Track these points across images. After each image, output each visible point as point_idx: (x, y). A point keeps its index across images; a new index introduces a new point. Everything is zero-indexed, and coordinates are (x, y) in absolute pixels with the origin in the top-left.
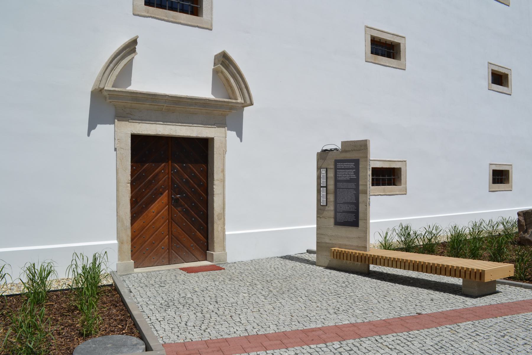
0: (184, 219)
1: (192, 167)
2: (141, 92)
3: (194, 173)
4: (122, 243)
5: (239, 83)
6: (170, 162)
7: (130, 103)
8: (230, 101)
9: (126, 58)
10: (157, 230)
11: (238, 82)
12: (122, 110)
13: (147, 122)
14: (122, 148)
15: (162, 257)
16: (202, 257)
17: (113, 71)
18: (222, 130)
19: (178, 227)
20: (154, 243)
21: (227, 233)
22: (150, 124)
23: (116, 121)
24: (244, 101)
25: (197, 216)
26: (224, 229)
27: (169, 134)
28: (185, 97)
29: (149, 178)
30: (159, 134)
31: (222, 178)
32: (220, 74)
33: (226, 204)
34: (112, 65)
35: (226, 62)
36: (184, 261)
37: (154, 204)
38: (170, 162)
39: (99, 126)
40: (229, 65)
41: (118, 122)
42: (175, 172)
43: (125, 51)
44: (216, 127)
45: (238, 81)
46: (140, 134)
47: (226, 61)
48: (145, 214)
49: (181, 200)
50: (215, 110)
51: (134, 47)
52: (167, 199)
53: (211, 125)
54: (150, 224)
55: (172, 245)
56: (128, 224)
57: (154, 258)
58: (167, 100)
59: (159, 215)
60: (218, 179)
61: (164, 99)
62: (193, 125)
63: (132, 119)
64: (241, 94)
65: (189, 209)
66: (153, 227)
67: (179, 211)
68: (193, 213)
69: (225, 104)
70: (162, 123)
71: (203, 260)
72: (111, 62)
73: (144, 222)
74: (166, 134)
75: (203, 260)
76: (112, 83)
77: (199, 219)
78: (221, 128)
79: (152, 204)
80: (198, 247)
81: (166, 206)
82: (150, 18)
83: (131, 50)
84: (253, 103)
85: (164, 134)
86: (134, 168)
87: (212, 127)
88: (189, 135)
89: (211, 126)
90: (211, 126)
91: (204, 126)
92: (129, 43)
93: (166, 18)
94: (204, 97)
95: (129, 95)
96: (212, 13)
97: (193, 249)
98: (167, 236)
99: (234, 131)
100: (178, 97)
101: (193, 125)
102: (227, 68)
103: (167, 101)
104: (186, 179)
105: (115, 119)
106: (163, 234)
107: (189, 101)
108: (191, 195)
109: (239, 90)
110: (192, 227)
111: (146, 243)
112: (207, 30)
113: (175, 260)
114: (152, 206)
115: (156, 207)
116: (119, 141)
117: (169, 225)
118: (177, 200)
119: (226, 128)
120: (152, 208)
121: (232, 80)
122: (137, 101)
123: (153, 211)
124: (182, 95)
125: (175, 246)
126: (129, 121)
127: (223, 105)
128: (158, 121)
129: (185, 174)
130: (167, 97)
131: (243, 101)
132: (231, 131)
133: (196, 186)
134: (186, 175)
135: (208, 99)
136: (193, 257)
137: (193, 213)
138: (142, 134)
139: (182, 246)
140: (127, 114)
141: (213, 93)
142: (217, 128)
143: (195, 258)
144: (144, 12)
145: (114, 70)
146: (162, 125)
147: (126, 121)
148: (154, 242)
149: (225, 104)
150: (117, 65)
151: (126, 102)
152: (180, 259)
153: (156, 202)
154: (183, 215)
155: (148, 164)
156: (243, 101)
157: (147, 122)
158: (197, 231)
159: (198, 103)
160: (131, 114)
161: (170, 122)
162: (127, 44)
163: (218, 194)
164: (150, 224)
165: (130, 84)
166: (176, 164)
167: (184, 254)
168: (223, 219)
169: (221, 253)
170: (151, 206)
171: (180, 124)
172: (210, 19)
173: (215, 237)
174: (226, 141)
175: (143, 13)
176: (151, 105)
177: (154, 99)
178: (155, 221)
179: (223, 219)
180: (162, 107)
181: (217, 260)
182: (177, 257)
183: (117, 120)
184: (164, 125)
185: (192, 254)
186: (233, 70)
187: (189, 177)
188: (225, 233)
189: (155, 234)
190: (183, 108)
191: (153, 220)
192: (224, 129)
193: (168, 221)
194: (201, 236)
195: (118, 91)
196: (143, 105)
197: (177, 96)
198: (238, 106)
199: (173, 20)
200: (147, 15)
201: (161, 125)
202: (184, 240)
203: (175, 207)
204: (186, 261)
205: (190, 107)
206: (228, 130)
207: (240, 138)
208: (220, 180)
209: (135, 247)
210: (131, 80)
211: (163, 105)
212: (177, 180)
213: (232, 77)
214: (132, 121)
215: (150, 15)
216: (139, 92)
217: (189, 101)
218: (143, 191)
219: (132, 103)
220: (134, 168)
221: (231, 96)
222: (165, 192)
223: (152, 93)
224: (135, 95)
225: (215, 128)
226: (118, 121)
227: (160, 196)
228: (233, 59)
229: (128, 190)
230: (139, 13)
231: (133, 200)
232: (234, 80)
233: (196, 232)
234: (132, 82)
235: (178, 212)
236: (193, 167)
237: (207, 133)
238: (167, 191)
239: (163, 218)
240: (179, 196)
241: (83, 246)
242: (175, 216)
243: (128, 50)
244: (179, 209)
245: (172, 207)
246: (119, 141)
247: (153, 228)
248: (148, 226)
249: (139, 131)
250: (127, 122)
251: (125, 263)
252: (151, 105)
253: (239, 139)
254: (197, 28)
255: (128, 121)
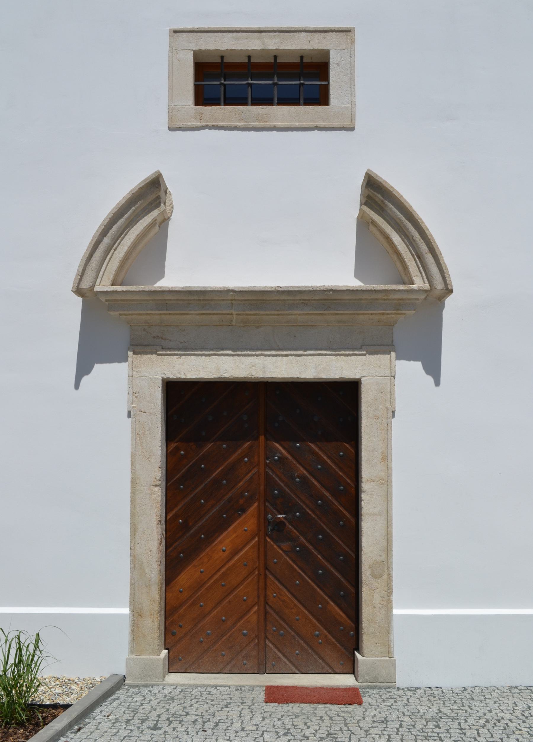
0: (296, 570)
1: (317, 450)
2: (171, 290)
3: (323, 463)
4: (140, 616)
5: (413, 242)
6: (262, 438)
7: (157, 314)
8: (389, 288)
9: (141, 221)
10: (232, 592)
11: (412, 241)
12: (144, 330)
13: (196, 353)
14: (143, 410)
15: (244, 653)
16: (342, 665)
17: (112, 251)
18: (384, 359)
19: (281, 587)
20: (223, 621)
21: (396, 612)
22: (204, 357)
23: (130, 353)
24: (430, 286)
25: (329, 566)
26: (390, 601)
27: (249, 376)
28: (274, 289)
29: (214, 475)
30: (225, 378)
31: (383, 474)
32: (372, 227)
33: (394, 539)
34: (106, 240)
35: (376, 196)
36: (296, 668)
37: (226, 533)
38: (262, 438)
39: (98, 368)
40: (384, 203)
41: (135, 356)
42: (275, 461)
43: (133, 208)
44: (365, 352)
45: (411, 237)
46: (183, 378)
47: (375, 193)
48: (204, 554)
49: (290, 527)
50: (358, 314)
51: (154, 196)
52: (256, 522)
53: (353, 349)
54: (215, 577)
55: (267, 628)
56: (153, 575)
57: (223, 656)
58: (236, 300)
59: (236, 558)
60: (373, 478)
61: (228, 300)
62: (305, 353)
63: (163, 349)
64: (421, 269)
65: (310, 547)
66: (223, 583)
67: (284, 551)
68: (319, 556)
69: (379, 296)
70: (230, 352)
71: (345, 671)
72: (104, 233)
73: (201, 572)
74: (242, 376)
75: (345, 671)
76: (111, 277)
77: (336, 574)
78: (380, 356)
79: (221, 533)
80: (333, 640)
81: (253, 538)
82: (207, 131)
83: (150, 204)
84: (451, 285)
85: (236, 376)
86: (182, 452)
87: (356, 355)
88: (296, 376)
89: (351, 353)
90: (351, 353)
91: (333, 353)
92: (142, 188)
93: (241, 124)
94: (322, 284)
95: (148, 298)
96: (353, 90)
97: (320, 644)
98: (256, 608)
99: (415, 360)
100: (255, 291)
101: (305, 353)
102: (380, 210)
103: (234, 302)
104: (303, 478)
105: (129, 349)
106: (245, 601)
107: (284, 297)
108: (315, 514)
109: (415, 260)
110: (318, 590)
111: (207, 619)
112: (343, 132)
113: (273, 666)
114: (221, 537)
115: (230, 540)
116: (136, 397)
117: (258, 582)
118: (279, 525)
119: (393, 354)
120: (220, 542)
121: (396, 238)
122: (167, 310)
123: (224, 548)
124: (265, 287)
125: (274, 630)
126: (158, 353)
127: (377, 299)
128: (223, 349)
129: (298, 466)
130: (231, 293)
131: (427, 286)
132: (409, 359)
133: (327, 494)
134: (302, 469)
135: (332, 290)
136: (321, 661)
137: (319, 556)
138: (186, 378)
139: (293, 633)
140: (154, 337)
141: (358, 275)
142: (367, 356)
143: (323, 664)
144: (193, 119)
145: (115, 250)
146: (232, 358)
147: (152, 354)
148: (224, 618)
149: (379, 296)
150: (120, 239)
151: (147, 314)
152: (286, 663)
153: (230, 529)
154: (294, 562)
155: (212, 444)
156: (427, 286)
157: (196, 353)
158: (329, 600)
159: (309, 300)
160: (163, 339)
161: (250, 349)
162: (135, 191)
163: (373, 514)
164: (215, 577)
165: (161, 275)
166: (277, 442)
167: (297, 652)
168: (385, 577)
169: (380, 661)
170: (217, 538)
171: (273, 352)
172: (348, 105)
173: (363, 619)
174: (393, 385)
175: (190, 122)
176: (203, 314)
177: (203, 300)
178: (227, 570)
179: (385, 577)
180: (228, 316)
181: (367, 678)
182: (279, 658)
183: (132, 353)
184: (236, 357)
185: (317, 654)
186: (395, 213)
187: (310, 473)
188: (392, 611)
189: (227, 600)
190: (278, 315)
191: (224, 569)
192: (387, 357)
193: (257, 572)
194: (341, 613)
195: (123, 291)
196: (185, 316)
197: (254, 290)
198: (418, 299)
199: (258, 123)
200: (199, 124)
201: (227, 357)
202: (297, 620)
203: (275, 541)
204: (301, 669)
205: (291, 312)
206: (398, 358)
207: (433, 377)
208: (377, 480)
209: (181, 627)
210: (164, 267)
211: (229, 312)
212: (281, 479)
213: (396, 231)
214: (164, 352)
215: (204, 124)
216: (167, 289)
217: (284, 297)
218: (202, 504)
219: (161, 314)
220: (182, 452)
221: (406, 278)
222: (250, 506)
223: (195, 289)
224: (160, 298)
225: (364, 355)
226: (135, 353)
227: (240, 516)
228: (393, 188)
229: (154, 500)
230: (181, 124)
231: (179, 523)
232: (401, 237)
233: (328, 603)
234: (166, 270)
235: (283, 554)
236: (320, 448)
237: (342, 368)
238: (256, 504)
239: (245, 565)
240: (284, 516)
241: (436, 615)
242: (275, 563)
243: (141, 204)
244: (285, 545)
245: (269, 540)
246: (136, 397)
247: (223, 586)
248: (212, 581)
249: (179, 373)
250: (154, 355)
251: (143, 658)
252: (203, 314)
253: (430, 379)
254: (316, 131)
255: (156, 353)
